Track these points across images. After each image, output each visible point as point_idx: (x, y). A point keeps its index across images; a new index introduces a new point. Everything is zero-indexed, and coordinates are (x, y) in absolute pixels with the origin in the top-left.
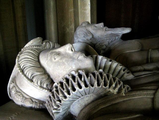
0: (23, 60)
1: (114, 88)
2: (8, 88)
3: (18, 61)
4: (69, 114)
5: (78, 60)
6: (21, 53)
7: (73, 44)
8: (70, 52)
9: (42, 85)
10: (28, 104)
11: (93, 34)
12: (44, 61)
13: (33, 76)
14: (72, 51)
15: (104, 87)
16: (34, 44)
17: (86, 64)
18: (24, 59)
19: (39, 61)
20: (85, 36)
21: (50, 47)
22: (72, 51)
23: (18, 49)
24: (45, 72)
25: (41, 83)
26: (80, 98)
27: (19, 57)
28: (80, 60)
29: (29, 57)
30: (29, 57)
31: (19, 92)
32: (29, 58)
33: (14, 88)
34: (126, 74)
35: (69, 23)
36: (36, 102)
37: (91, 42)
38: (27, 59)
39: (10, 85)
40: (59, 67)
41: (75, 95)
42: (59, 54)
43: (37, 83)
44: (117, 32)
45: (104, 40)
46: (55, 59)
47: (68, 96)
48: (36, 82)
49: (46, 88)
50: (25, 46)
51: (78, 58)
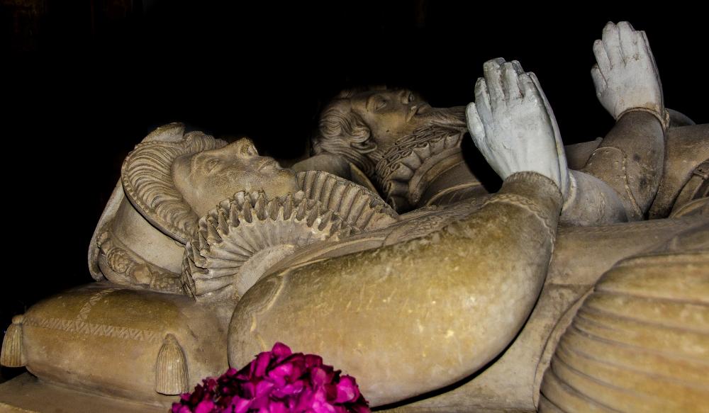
0: (138, 168)
1: (321, 227)
2: (90, 251)
5: (259, 175)
6: (134, 155)
7: (216, 116)
9: (175, 223)
12: (182, 179)
13: (157, 201)
15: (296, 221)
20: (345, 133)
25: (173, 219)
26: (255, 256)
28: (266, 175)
30: (149, 162)
31: (122, 251)
32: (150, 166)
37: (365, 155)
38: (146, 167)
40: (216, 187)
45: (403, 147)
49: (184, 230)
51: (261, 171)
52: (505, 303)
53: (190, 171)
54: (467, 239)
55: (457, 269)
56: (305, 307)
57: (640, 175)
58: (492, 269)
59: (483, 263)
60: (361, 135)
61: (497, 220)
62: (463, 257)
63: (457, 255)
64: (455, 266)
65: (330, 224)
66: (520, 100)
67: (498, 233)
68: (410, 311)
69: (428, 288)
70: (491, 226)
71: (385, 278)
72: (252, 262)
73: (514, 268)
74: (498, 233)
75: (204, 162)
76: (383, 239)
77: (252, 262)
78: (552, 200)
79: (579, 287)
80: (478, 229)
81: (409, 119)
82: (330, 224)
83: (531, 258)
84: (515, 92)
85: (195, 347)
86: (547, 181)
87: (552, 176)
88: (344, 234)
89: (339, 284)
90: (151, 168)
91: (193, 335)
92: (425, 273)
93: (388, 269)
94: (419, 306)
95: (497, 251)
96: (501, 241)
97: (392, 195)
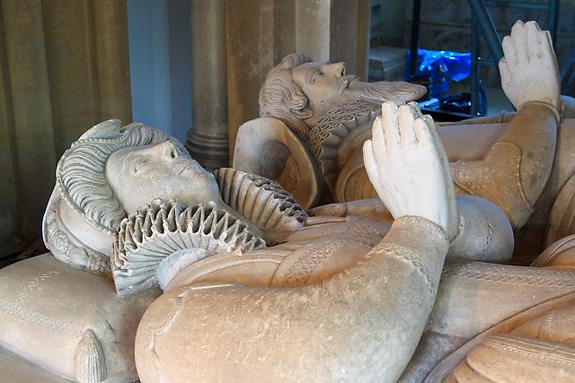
3: (61, 170)
4: (153, 286)
5: (180, 178)
8: (169, 160)
10: (79, 260)
11: (311, 97)
13: (85, 201)
14: (173, 156)
16: (101, 133)
17: (194, 187)
18: (72, 169)
19: (104, 172)
21: (139, 142)
22: (173, 156)
23: (61, 148)
24: (113, 196)
26: (171, 255)
27: (63, 161)
28: (186, 179)
29: (82, 162)
30: (82, 162)
31: (63, 233)
32: (82, 166)
33: (54, 224)
34: (285, 218)
35: (260, 48)
36: (94, 258)
39: (48, 217)
41: (151, 244)
42: (145, 161)
43: (92, 215)
44: (374, 98)
46: (136, 171)
47: (138, 244)
48: (90, 214)
50: (81, 138)
52: (376, 373)
53: (119, 171)
54: (344, 303)
55: (330, 338)
56: (193, 344)
57: (531, 172)
58: (366, 340)
59: (356, 333)
60: (298, 101)
61: (378, 280)
62: (337, 325)
63: (333, 322)
64: (328, 336)
65: (235, 238)
66: (414, 145)
67: (376, 297)
68: (283, 375)
69: (301, 355)
70: (370, 289)
71: (262, 335)
72: (169, 260)
73: (388, 335)
74: (376, 297)
75: (132, 162)
76: (279, 262)
77: (169, 260)
78: (437, 248)
79: (456, 337)
80: (357, 291)
81: (340, 92)
82: (235, 238)
83: (407, 323)
84: (409, 136)
85: (113, 339)
86: (434, 229)
87: (440, 222)
88: (247, 248)
89: (222, 329)
90: (83, 168)
91: (111, 329)
92: (300, 340)
93: (266, 326)
94: (291, 371)
95: (372, 320)
96: (379, 307)
97: (322, 159)
